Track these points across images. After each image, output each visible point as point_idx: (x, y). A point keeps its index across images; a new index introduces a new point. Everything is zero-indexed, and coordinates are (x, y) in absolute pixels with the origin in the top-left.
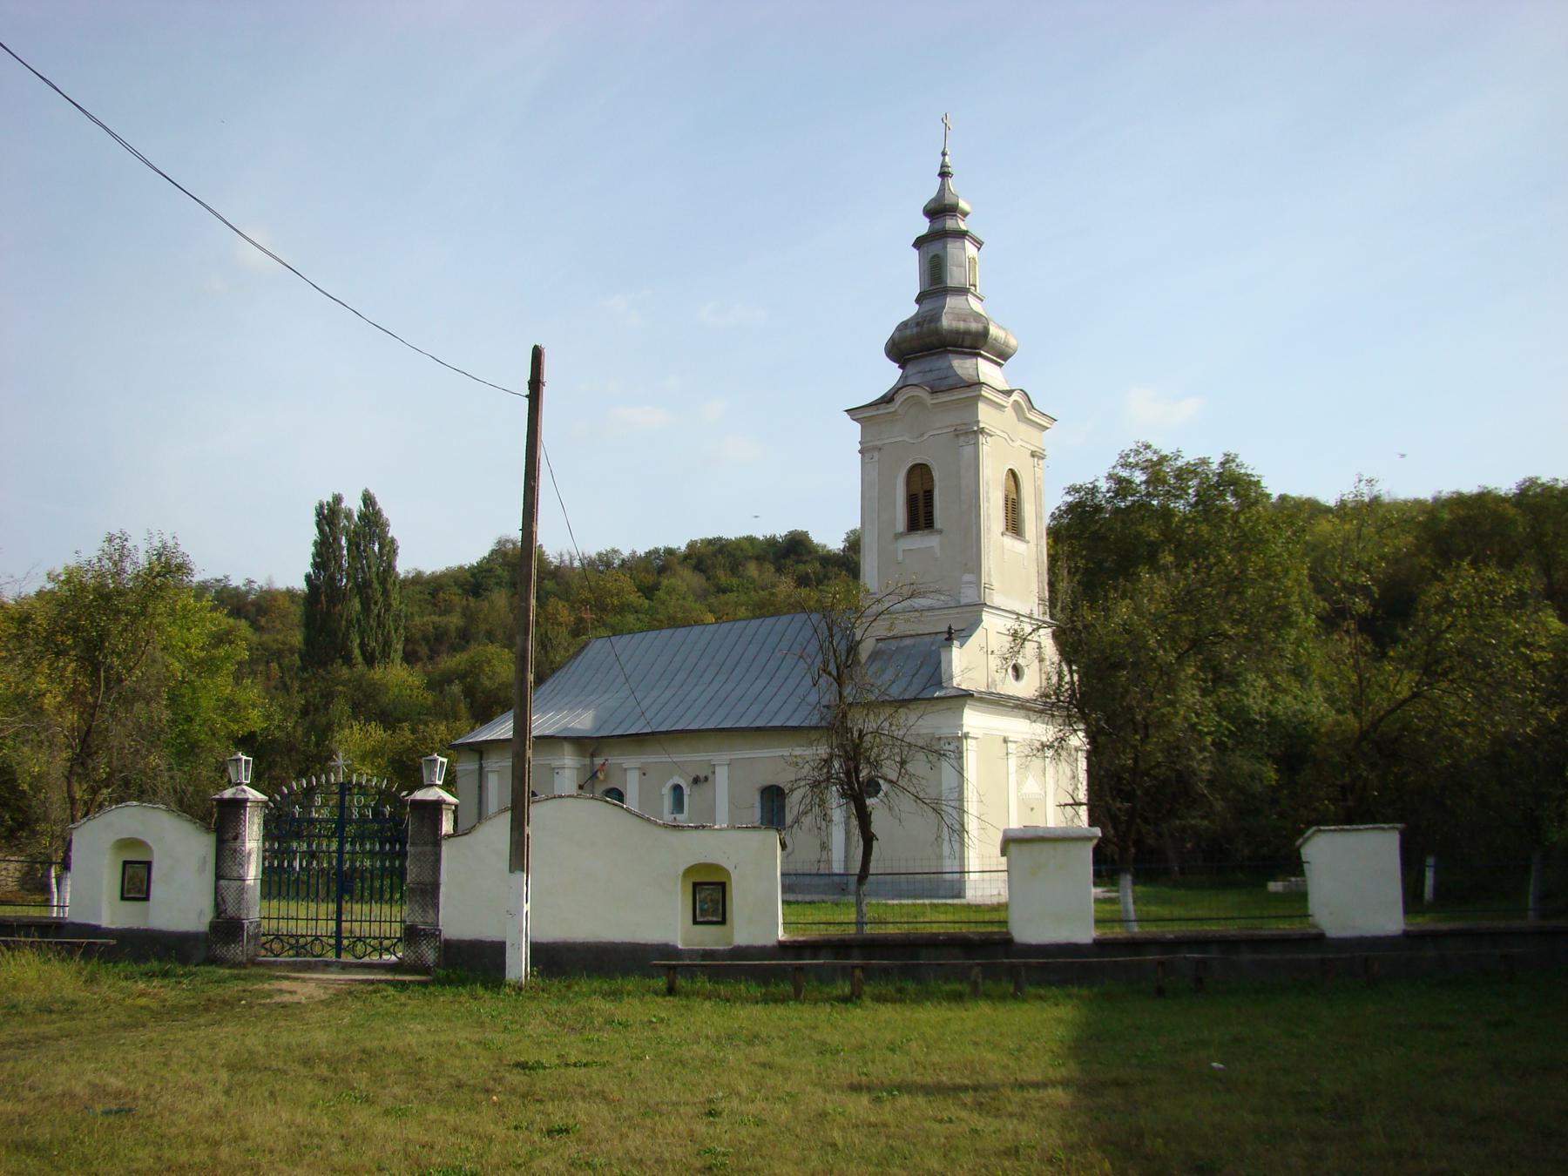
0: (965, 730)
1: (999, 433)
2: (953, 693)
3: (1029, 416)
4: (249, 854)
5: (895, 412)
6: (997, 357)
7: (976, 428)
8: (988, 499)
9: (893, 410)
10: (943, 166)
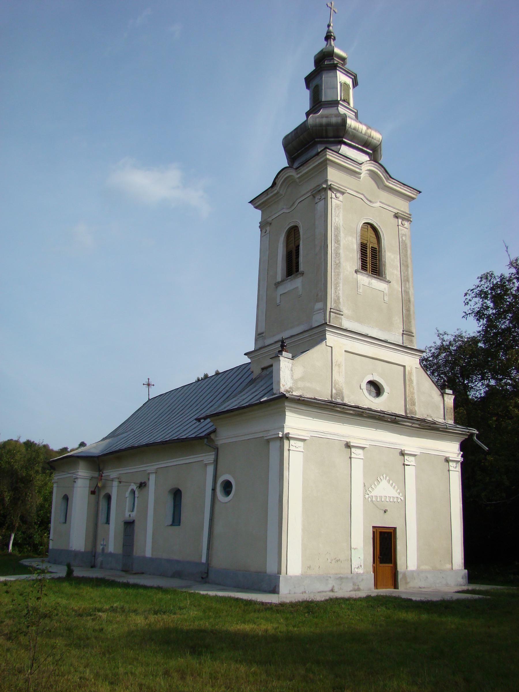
0: (286, 431)
1: (349, 191)
2: (266, 395)
3: (387, 184)
4: (479, 597)
5: (278, 193)
6: (363, 146)
7: (324, 186)
8: (338, 242)
9: (275, 192)
10: (329, 32)
